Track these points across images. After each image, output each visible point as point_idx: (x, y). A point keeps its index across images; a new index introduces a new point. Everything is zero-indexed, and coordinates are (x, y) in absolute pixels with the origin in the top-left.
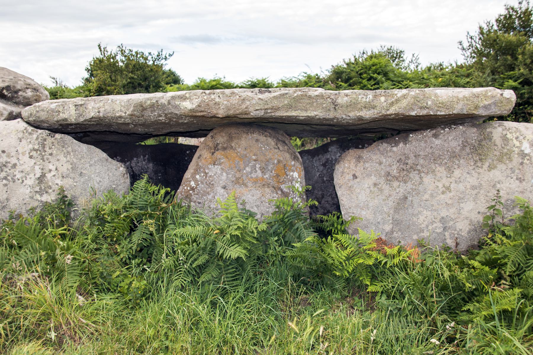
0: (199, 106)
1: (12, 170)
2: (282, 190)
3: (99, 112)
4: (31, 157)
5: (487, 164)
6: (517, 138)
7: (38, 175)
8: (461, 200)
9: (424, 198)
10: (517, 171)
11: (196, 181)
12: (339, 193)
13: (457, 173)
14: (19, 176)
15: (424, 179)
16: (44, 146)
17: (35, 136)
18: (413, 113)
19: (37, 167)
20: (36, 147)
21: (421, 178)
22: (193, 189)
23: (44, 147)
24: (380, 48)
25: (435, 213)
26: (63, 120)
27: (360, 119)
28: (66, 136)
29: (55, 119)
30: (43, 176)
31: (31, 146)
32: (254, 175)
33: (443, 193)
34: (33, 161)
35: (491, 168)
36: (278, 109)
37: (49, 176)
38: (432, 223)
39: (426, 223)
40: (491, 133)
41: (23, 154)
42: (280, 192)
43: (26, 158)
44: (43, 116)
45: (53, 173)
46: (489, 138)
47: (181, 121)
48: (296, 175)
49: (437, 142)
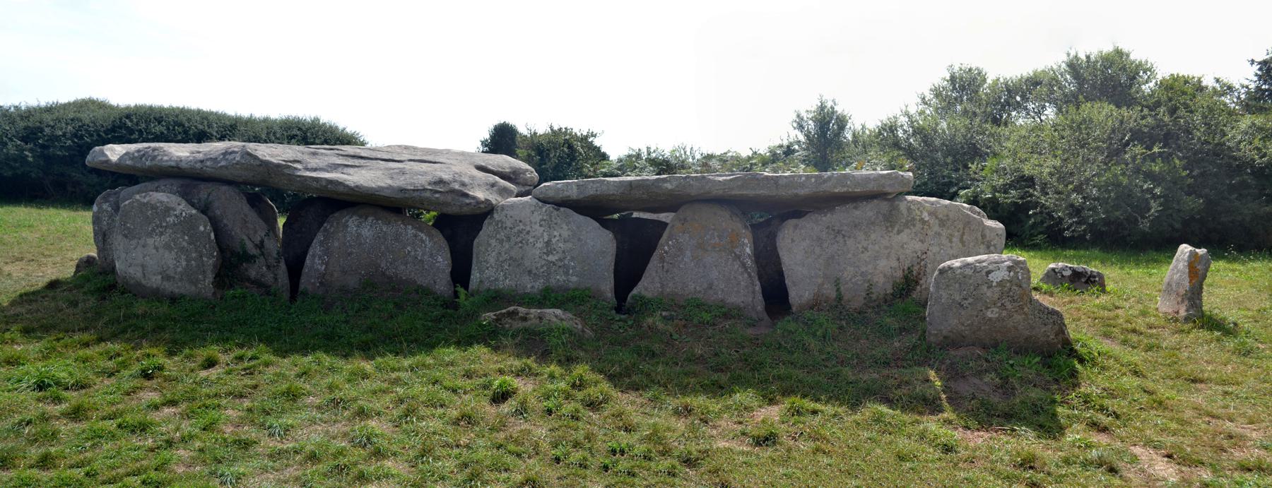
0: (677, 187)
1: (527, 236)
2: (735, 253)
3: (597, 191)
4: (541, 226)
5: (896, 229)
6: (918, 209)
7: (546, 240)
8: (876, 258)
9: (848, 257)
10: (919, 234)
11: (669, 246)
12: (781, 254)
13: (873, 236)
14: (531, 240)
15: (847, 242)
16: (551, 217)
17: (544, 209)
18: (837, 191)
19: (545, 234)
20: (545, 218)
21: (845, 241)
22: (666, 252)
23: (551, 218)
24: (849, 115)
25: (857, 269)
26: (566, 197)
27: (796, 195)
28: (568, 209)
29: (561, 196)
30: (549, 241)
31: (541, 217)
32: (713, 242)
33: (863, 252)
34: (543, 229)
35: (899, 232)
36: (733, 189)
37: (554, 240)
38: (855, 276)
39: (850, 277)
40: (899, 205)
41: (535, 223)
42: (733, 255)
43: (537, 226)
44: (551, 194)
45: (557, 238)
46: (897, 208)
47: (659, 198)
48: (746, 241)
49: (857, 212)
